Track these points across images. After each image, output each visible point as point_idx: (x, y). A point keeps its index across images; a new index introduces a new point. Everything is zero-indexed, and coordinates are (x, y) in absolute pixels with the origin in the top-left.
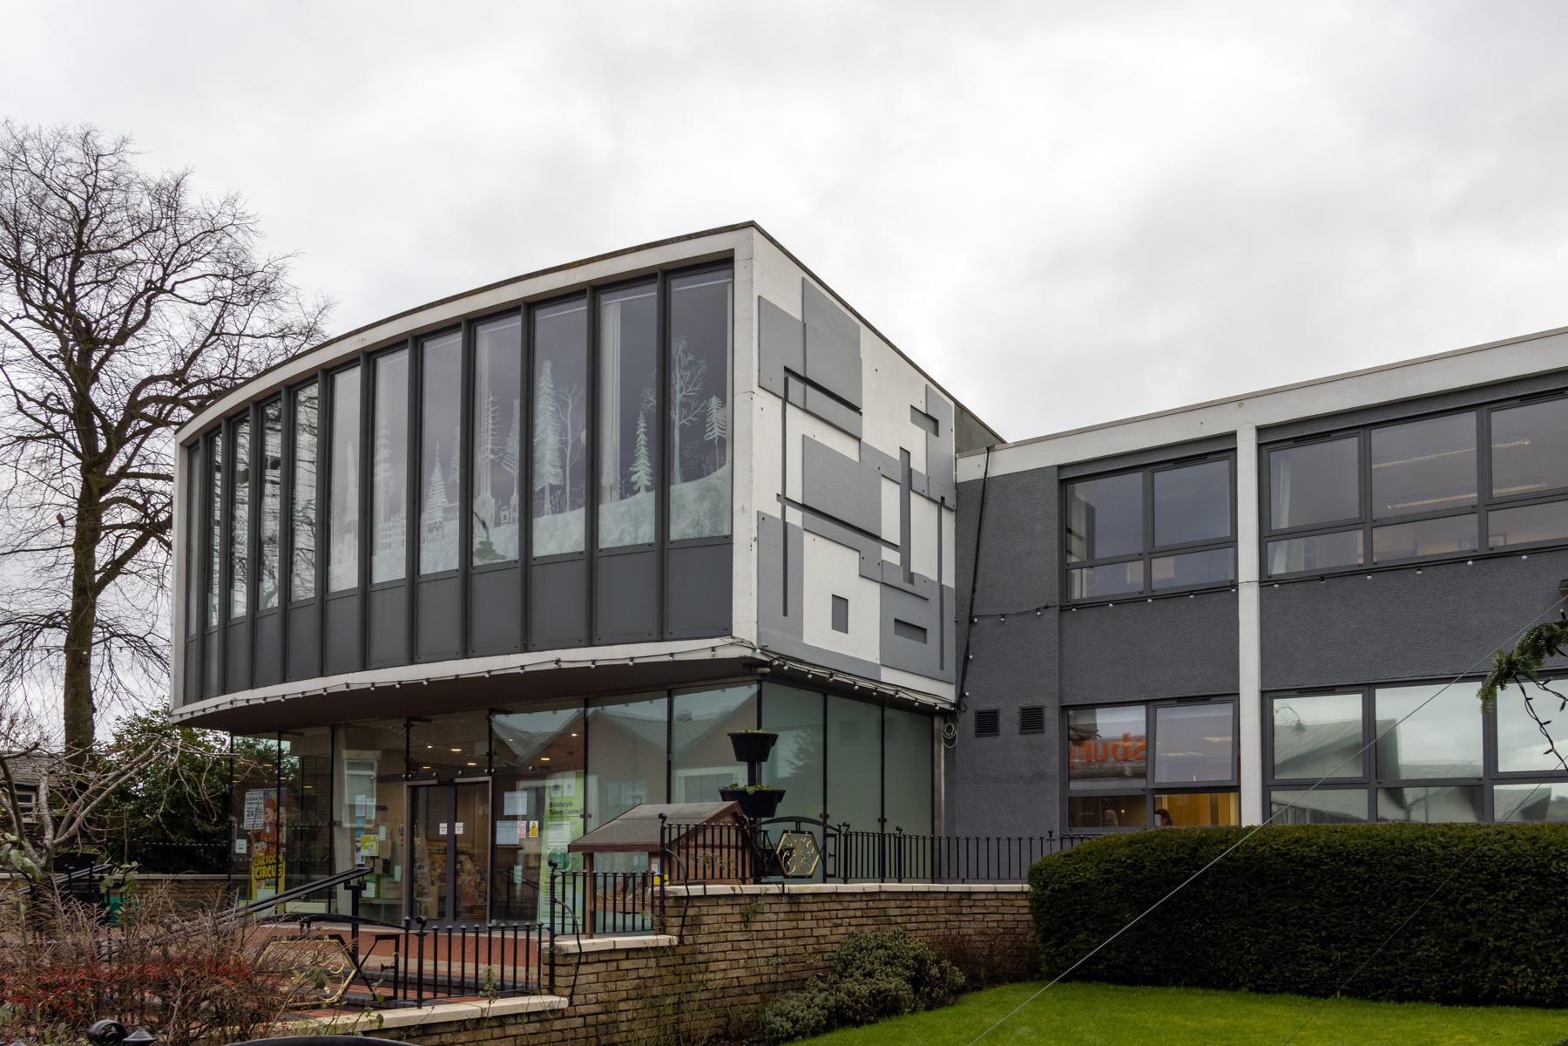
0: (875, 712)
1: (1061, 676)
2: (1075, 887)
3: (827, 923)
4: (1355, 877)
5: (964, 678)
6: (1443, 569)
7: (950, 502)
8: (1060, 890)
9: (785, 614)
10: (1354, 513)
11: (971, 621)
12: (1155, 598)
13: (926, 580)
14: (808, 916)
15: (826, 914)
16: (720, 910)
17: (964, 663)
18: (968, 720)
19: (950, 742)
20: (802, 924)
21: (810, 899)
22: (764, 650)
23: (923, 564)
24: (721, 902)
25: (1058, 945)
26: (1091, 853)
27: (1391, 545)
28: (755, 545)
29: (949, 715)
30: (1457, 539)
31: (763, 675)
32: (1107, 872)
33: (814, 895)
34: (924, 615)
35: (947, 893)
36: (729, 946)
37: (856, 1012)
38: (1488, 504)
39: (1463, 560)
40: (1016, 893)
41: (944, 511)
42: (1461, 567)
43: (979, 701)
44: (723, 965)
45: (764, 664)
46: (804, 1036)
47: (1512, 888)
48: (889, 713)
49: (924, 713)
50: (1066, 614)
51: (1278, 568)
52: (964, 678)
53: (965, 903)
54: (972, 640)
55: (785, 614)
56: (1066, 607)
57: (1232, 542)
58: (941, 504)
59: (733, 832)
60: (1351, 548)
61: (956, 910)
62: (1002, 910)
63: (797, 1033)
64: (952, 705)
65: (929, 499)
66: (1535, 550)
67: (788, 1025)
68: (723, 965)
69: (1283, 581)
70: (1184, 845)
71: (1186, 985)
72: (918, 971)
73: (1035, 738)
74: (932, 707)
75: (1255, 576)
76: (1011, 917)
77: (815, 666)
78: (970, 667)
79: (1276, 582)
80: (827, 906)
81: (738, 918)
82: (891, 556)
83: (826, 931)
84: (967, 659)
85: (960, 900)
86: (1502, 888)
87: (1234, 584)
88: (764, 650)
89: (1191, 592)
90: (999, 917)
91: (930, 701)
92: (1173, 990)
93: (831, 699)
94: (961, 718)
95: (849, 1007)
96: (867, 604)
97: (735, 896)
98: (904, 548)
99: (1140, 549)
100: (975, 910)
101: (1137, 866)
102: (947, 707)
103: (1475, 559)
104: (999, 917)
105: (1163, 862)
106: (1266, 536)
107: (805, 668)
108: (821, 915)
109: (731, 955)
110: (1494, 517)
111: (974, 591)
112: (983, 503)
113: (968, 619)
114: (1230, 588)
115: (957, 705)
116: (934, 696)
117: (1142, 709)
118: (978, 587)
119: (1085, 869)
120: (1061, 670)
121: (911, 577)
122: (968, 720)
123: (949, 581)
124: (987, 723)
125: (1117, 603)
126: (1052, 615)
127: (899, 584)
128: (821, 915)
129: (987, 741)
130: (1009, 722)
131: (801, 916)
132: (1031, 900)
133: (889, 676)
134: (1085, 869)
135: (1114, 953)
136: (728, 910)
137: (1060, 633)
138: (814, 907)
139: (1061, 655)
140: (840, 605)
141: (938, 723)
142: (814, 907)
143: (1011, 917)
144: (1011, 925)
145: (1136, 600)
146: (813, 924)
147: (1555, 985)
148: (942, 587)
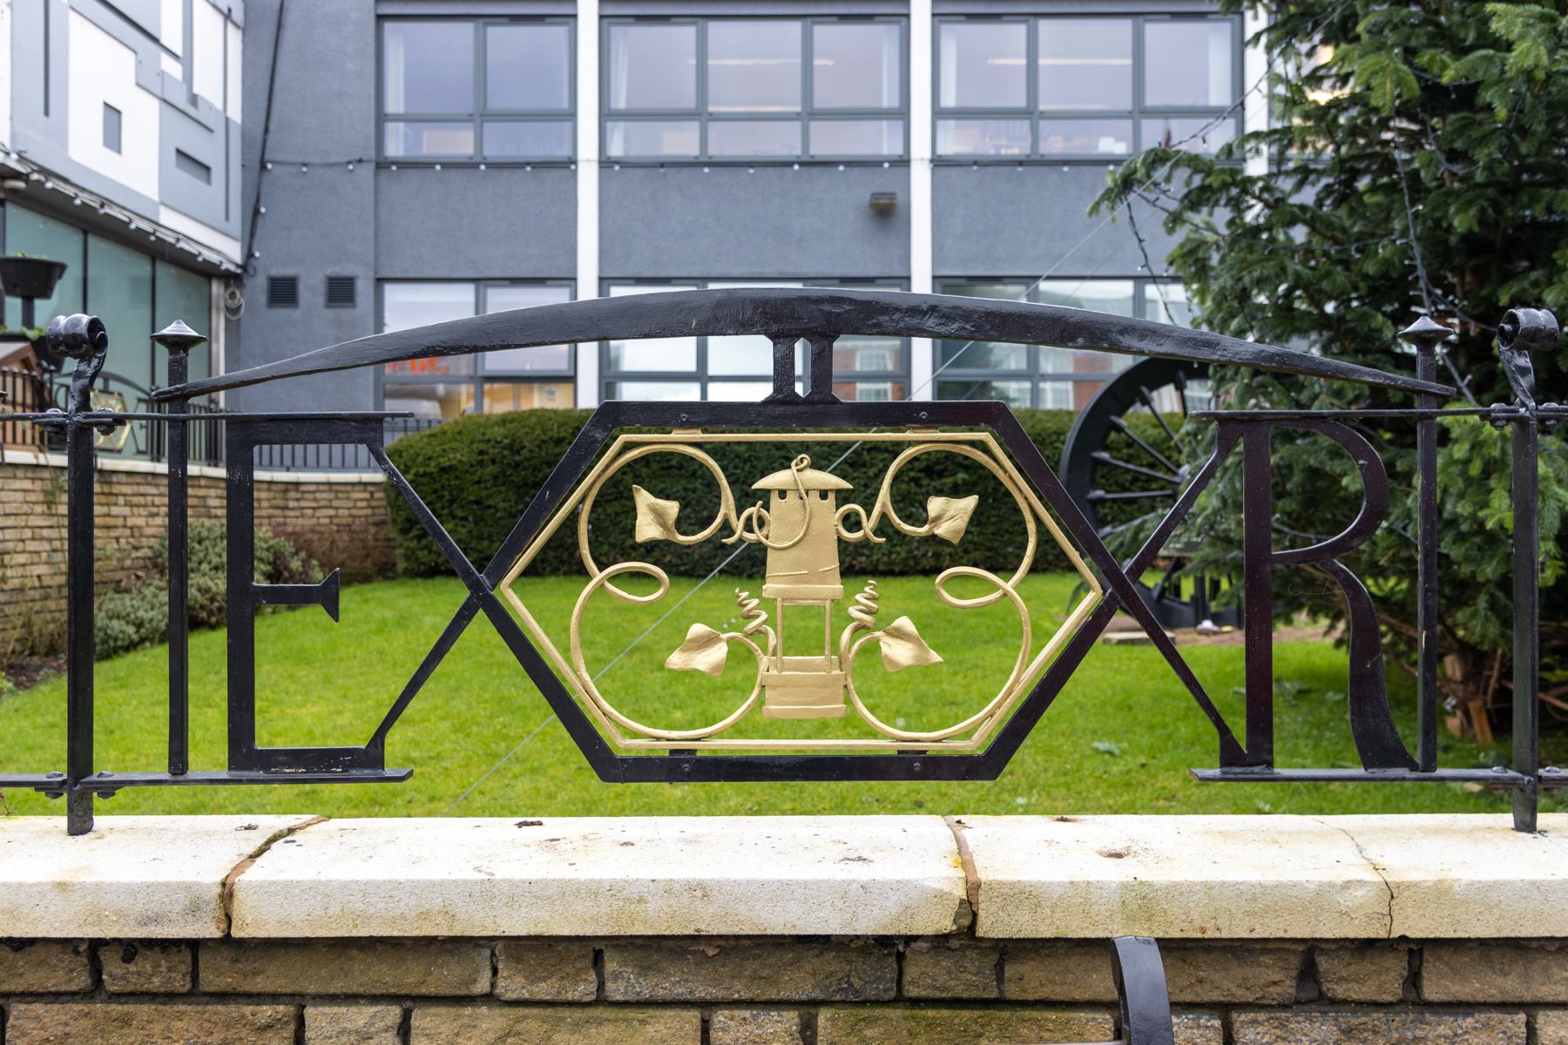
0: (142, 267)
1: (377, 243)
2: (444, 470)
3: (143, 511)
4: (737, 456)
5: (252, 234)
6: (771, 170)
7: (238, 16)
8: (425, 475)
9: (47, 113)
10: (690, 103)
11: (263, 167)
12: (490, 165)
13: (211, 107)
14: (121, 500)
15: (141, 500)
16: (18, 484)
17: (254, 215)
18: (258, 287)
19: (232, 311)
20: (115, 510)
21: (124, 478)
22: (22, 159)
23: (207, 85)
24: (20, 473)
25: (419, 538)
26: (460, 433)
27: (728, 143)
28: (7, 11)
29: (231, 279)
30: (783, 142)
31: (15, 191)
32: (481, 453)
33: (129, 473)
34: (208, 150)
35: (271, 483)
36: (28, 533)
37: (211, 613)
38: (810, 114)
39: (789, 164)
40: (353, 484)
41: (230, 25)
42: (787, 170)
43: (272, 265)
44: (21, 559)
45: (18, 176)
46: (152, 641)
47: (872, 465)
48: (163, 271)
49: (206, 272)
50: (384, 174)
51: (616, 150)
52: (252, 234)
53: (292, 495)
54: (264, 190)
55: (47, 113)
56: (382, 165)
57: (571, 115)
58: (227, 16)
59: (19, 382)
60: (680, 141)
61: (281, 503)
62: (335, 503)
63: (142, 640)
64: (238, 266)
65: (215, 6)
66: (851, 163)
67: (131, 630)
68: (21, 559)
69: (624, 164)
70: (565, 424)
71: (565, 574)
72: (273, 564)
73: (344, 313)
74: (217, 266)
75: (594, 155)
76: (346, 512)
77: (84, 190)
78: (260, 222)
79: (617, 163)
80: (142, 489)
81: (41, 498)
82: (173, 69)
83: (140, 521)
84: (256, 212)
85: (286, 491)
86: (864, 465)
87: (573, 161)
88: (22, 159)
89: (528, 164)
90: (331, 512)
91: (214, 258)
92: (552, 580)
93: (93, 241)
94: (248, 282)
95: (202, 607)
96: (144, 121)
97: (37, 466)
98: (186, 60)
99: (470, 110)
100: (303, 504)
101: (514, 447)
102: (232, 268)
103: (801, 164)
104: (331, 512)
105: (544, 442)
106: (607, 115)
107: (70, 191)
108: (135, 500)
109: (31, 546)
110: (815, 126)
111: (266, 130)
112: (279, 27)
113: (259, 165)
114: (568, 164)
115: (244, 267)
116: (218, 252)
117: (471, 288)
118: (272, 127)
119: (454, 450)
120: (376, 236)
121: (194, 100)
122: (258, 287)
123: (235, 114)
124: (283, 292)
125: (445, 165)
126: (367, 171)
127: (182, 107)
128: (135, 500)
129: (283, 313)
130: (311, 292)
131: (112, 499)
132: (385, 491)
133: (168, 218)
134: (454, 450)
135: (486, 543)
136: (27, 485)
137: (376, 192)
138: (127, 490)
139: (377, 218)
140: (112, 113)
141: (217, 288)
142: (127, 490)
143: (346, 512)
144: (344, 521)
145: (469, 165)
146: (126, 511)
147: (903, 555)
148: (227, 119)
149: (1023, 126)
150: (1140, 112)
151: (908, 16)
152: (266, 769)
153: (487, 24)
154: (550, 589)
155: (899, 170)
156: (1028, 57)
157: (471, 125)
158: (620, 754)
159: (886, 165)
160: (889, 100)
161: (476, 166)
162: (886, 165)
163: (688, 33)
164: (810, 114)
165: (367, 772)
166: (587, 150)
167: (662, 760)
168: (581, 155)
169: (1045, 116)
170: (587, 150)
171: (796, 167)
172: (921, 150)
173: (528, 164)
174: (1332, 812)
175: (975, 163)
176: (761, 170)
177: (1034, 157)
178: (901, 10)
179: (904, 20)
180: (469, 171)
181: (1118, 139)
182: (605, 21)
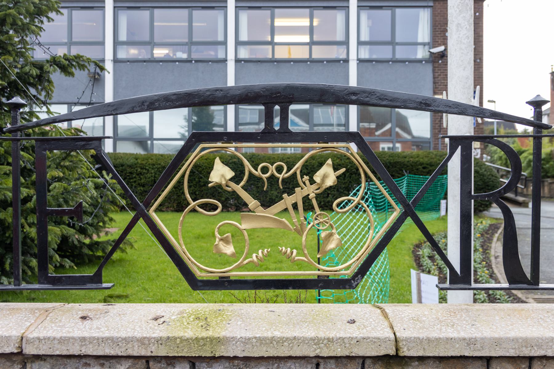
10: (389, 39)
30: (301, 53)
38: (70, 43)
69: (246, 61)
75: (233, 58)
114: (224, 61)
149: (390, 48)
150: (191, 43)
151: (348, 7)
152: (53, 284)
153: (193, 10)
154: (170, 216)
155: (345, 64)
156: (192, 25)
157: (66, 47)
158: (199, 279)
159: (193, 62)
160: (340, 37)
161: (191, 61)
162: (193, 62)
163: (388, 13)
164: (70, 43)
165: (94, 286)
166: (231, 56)
167: (217, 281)
168: (106, 58)
169: (398, 44)
170: (231, 56)
171: (243, 62)
172: (353, 56)
173: (210, 61)
174: (276, 280)
175: (128, 61)
176: (165, 64)
177: (273, 59)
178: (347, 5)
179: (347, 8)
180: (320, 64)
181: (184, 52)
182: (237, 9)
